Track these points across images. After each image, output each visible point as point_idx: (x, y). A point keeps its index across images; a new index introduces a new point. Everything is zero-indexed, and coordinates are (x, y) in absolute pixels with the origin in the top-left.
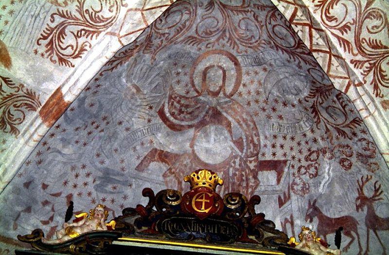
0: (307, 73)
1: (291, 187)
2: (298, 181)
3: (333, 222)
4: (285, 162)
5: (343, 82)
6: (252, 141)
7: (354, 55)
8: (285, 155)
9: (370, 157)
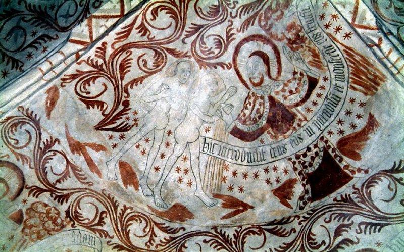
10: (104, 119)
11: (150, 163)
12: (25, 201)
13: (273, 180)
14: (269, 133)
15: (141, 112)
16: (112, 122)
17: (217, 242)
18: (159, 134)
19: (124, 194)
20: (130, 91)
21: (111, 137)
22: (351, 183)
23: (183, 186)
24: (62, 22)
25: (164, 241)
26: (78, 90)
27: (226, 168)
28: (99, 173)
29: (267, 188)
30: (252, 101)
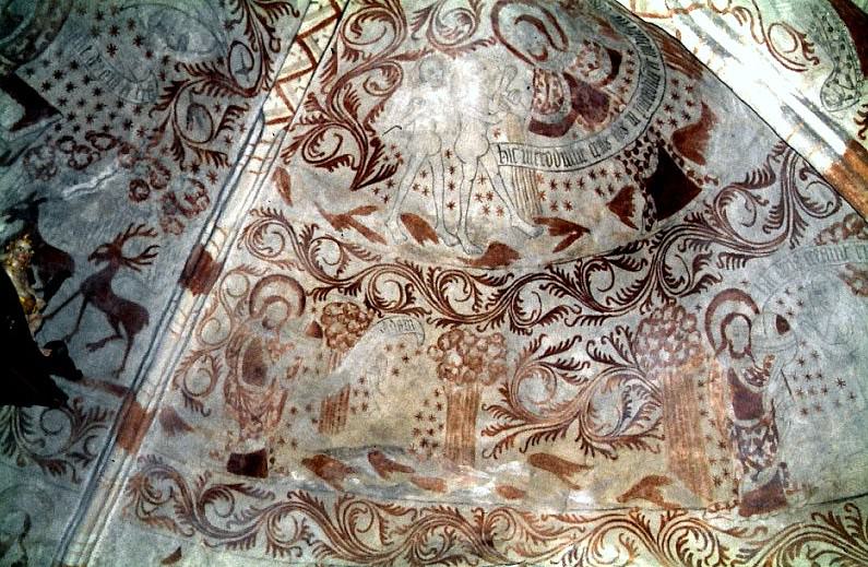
0: (230, 43)
1: (27, 152)
2: (46, 152)
3: (42, 245)
4: (52, 111)
5: (282, 111)
6: (33, 39)
7: (322, 91)
8: (63, 102)
9: (184, 212)
10: (356, 178)
11: (440, 204)
12: (314, 310)
13: (604, 188)
14: (580, 123)
15: (401, 143)
16: (368, 173)
17: (556, 286)
18: (436, 160)
19: (422, 254)
20: (373, 126)
21: (376, 191)
22: (701, 196)
23: (493, 216)
24: (244, 82)
25: (493, 298)
26: (308, 158)
27: (540, 179)
28: (381, 240)
29: (599, 200)
30: (542, 79)
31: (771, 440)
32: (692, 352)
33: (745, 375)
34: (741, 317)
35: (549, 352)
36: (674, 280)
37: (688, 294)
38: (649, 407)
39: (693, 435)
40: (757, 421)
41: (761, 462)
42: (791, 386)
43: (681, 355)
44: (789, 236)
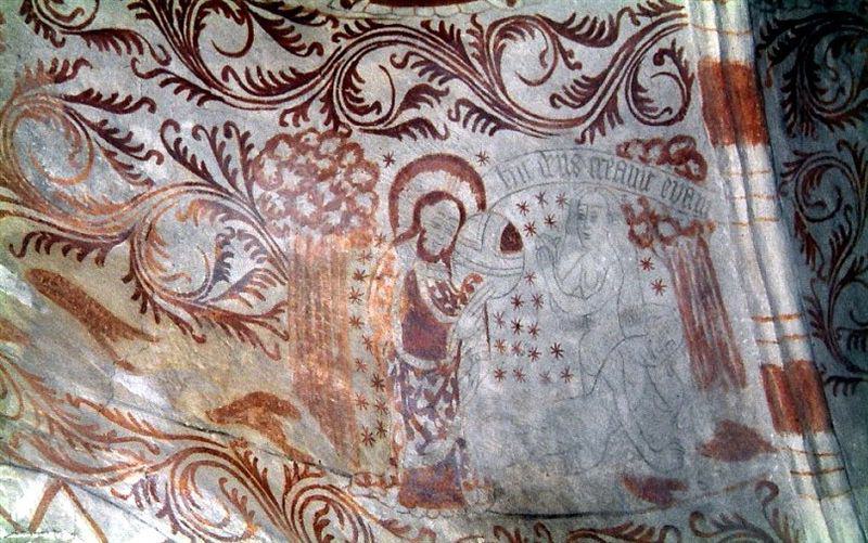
31: (448, 400)
32: (354, 221)
33: (431, 290)
34: (454, 204)
35: (88, 97)
36: (361, 100)
37: (376, 132)
38: (265, 278)
39: (335, 351)
40: (432, 365)
41: (433, 427)
42: (491, 333)
43: (335, 219)
44: (588, 123)
